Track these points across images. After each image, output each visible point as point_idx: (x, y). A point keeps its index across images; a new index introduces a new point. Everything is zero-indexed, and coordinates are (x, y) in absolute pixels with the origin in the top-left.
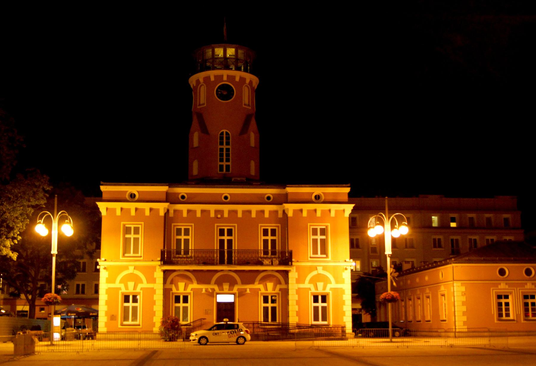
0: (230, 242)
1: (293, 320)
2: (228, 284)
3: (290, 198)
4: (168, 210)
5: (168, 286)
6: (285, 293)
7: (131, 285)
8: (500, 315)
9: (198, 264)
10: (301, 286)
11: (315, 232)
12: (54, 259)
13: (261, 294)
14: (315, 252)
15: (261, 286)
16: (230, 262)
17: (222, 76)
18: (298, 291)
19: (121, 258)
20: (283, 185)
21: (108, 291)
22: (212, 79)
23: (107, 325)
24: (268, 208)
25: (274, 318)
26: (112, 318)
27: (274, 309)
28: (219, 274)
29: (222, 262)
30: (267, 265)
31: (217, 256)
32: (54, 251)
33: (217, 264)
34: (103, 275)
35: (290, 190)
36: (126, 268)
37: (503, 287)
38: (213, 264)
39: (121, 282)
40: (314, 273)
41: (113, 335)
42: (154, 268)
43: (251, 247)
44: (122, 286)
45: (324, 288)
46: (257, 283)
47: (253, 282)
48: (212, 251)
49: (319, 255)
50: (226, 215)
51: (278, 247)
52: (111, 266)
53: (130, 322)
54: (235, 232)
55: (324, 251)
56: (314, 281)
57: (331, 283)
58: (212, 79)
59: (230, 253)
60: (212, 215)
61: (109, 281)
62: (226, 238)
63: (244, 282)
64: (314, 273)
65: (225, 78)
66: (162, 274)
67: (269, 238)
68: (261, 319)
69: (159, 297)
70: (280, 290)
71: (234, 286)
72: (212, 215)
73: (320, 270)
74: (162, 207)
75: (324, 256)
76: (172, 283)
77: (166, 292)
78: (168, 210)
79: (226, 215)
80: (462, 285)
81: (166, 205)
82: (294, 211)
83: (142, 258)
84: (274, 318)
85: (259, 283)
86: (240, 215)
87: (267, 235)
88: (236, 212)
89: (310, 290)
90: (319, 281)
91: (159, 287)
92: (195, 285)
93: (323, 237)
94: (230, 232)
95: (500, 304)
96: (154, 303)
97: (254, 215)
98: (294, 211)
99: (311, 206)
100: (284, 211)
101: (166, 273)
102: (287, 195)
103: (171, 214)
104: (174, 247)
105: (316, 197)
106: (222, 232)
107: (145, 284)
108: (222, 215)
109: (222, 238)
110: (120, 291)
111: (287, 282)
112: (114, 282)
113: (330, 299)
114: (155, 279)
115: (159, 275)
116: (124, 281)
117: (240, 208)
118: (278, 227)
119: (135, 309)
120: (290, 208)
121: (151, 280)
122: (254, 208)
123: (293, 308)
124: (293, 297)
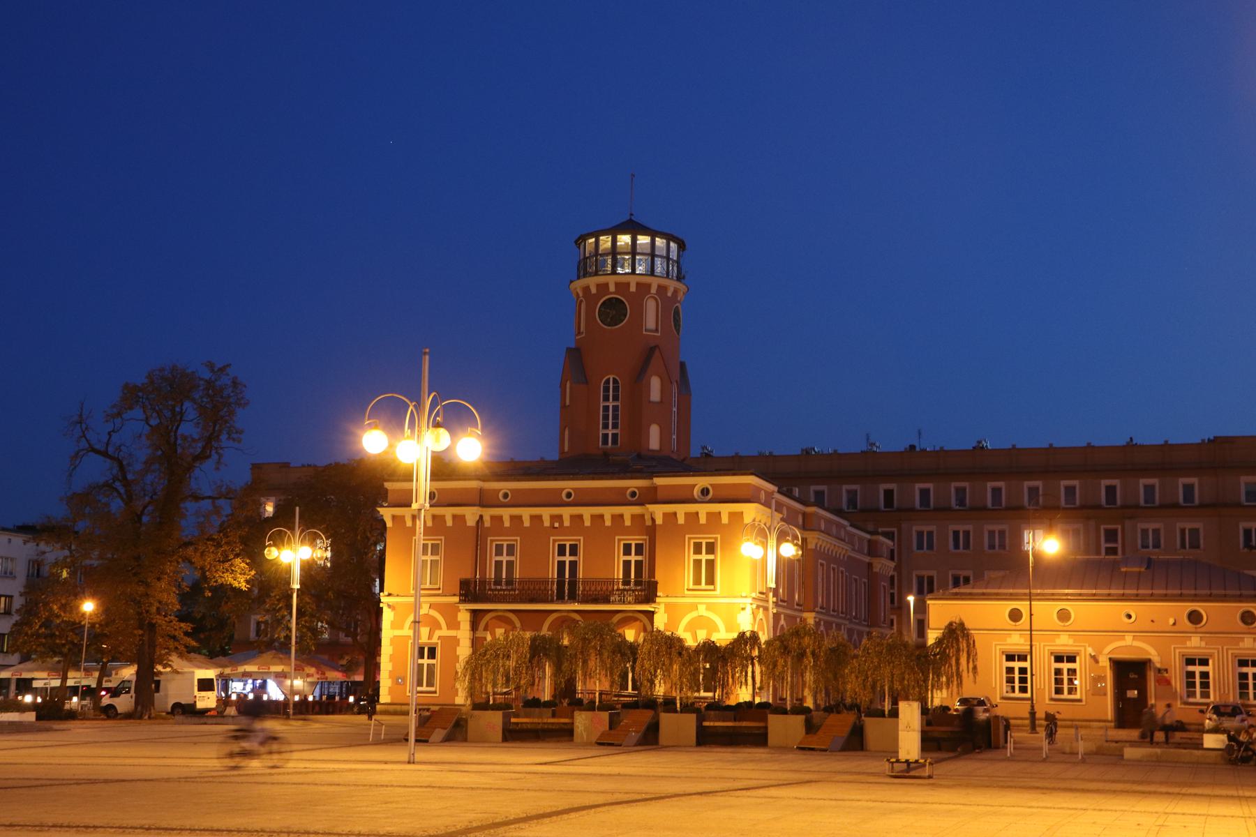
0: (573, 565)
3: (660, 495)
4: (481, 517)
5: (480, 634)
7: (424, 631)
8: (1059, 691)
9: (522, 601)
11: (698, 549)
12: (295, 595)
14: (697, 581)
16: (573, 598)
17: (607, 285)
20: (650, 476)
22: (594, 290)
23: (391, 691)
24: (628, 512)
26: (398, 680)
28: (554, 616)
29: (560, 598)
30: (614, 603)
32: (296, 586)
33: (552, 601)
34: (387, 617)
35: (659, 481)
37: (1195, 644)
40: (694, 614)
41: (274, 692)
43: (602, 575)
48: (546, 581)
49: (703, 586)
50: (567, 523)
52: (401, 604)
53: (424, 688)
55: (711, 580)
57: (718, 631)
58: (594, 290)
59: (573, 583)
60: (547, 523)
61: (394, 625)
62: (568, 559)
64: (694, 614)
65: (612, 288)
67: (633, 558)
72: (547, 523)
73: (702, 610)
74: (470, 515)
75: (711, 587)
76: (486, 629)
78: (481, 517)
79: (567, 523)
81: (475, 509)
82: (665, 515)
86: (587, 523)
87: (630, 554)
88: (580, 517)
90: (701, 628)
91: (464, 634)
93: (711, 557)
98: (665, 515)
99: (691, 508)
101: (476, 616)
102: (655, 489)
103: (487, 523)
105: (702, 491)
106: (562, 550)
107: (445, 632)
108: (561, 522)
109: (572, 558)
112: (401, 627)
114: (459, 623)
115: (464, 617)
117: (587, 512)
118: (619, 540)
120: (658, 511)
121: (453, 624)
122: (608, 512)
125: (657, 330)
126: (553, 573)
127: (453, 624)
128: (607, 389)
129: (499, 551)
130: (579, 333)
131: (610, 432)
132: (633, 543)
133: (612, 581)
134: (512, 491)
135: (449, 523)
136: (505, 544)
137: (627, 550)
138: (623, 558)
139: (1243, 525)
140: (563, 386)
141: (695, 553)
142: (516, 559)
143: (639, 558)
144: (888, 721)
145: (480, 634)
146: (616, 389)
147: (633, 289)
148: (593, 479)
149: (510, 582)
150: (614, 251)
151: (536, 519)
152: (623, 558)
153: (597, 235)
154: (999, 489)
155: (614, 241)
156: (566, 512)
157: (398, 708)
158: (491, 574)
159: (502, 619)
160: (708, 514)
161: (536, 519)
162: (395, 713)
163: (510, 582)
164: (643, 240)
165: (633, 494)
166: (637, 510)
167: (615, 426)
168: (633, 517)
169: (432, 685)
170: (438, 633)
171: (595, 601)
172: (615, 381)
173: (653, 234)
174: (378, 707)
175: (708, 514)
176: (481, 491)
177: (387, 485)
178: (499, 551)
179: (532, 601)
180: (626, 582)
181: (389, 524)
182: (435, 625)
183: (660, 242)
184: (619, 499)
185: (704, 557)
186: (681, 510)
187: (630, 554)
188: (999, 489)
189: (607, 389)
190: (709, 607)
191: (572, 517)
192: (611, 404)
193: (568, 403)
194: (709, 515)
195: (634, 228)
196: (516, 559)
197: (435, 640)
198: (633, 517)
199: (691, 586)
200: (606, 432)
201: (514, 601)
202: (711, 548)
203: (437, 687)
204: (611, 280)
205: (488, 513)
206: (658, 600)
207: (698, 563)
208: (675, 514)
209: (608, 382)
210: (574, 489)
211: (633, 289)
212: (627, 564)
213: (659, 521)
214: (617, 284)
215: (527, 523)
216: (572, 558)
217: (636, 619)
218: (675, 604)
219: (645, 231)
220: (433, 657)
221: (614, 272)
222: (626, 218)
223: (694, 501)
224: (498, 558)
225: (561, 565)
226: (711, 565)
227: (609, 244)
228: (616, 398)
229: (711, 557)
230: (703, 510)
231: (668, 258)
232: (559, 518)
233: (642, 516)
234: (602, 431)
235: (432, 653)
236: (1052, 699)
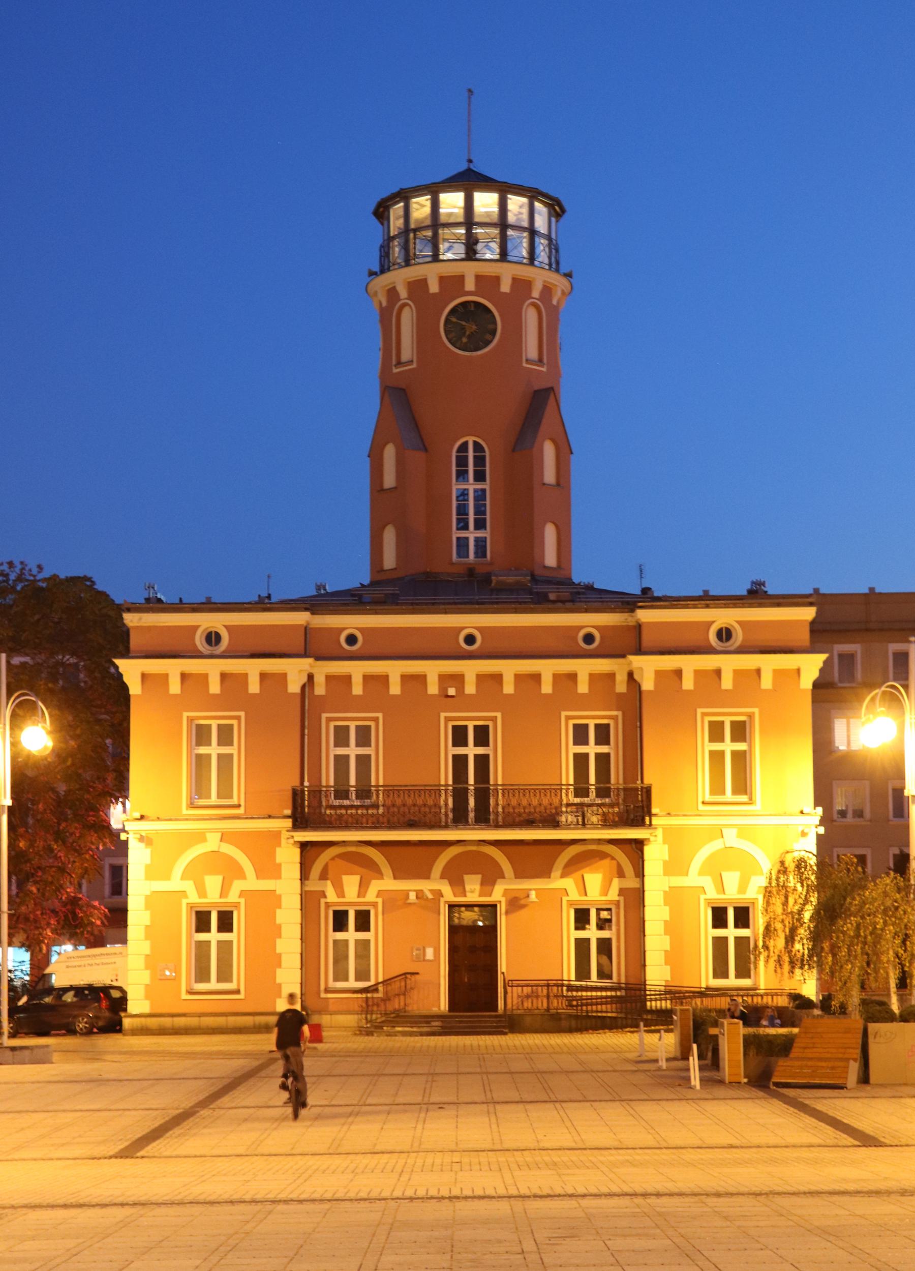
0: (482, 762)
2: (479, 877)
3: (647, 639)
4: (311, 677)
5: (313, 885)
7: (213, 883)
10: (678, 881)
11: (716, 732)
13: (571, 903)
14: (717, 787)
15: (568, 883)
16: (483, 818)
19: (185, 811)
21: (151, 901)
29: (460, 818)
30: (568, 827)
34: (138, 860)
36: (201, 837)
40: (716, 845)
42: (275, 837)
44: (189, 886)
45: (743, 888)
46: (556, 872)
47: (545, 873)
48: (435, 791)
49: (729, 796)
50: (470, 688)
51: (616, 777)
53: (213, 985)
54: (378, 735)
55: (743, 785)
58: (434, 288)
59: (483, 795)
61: (151, 873)
62: (471, 751)
63: (520, 874)
64: (716, 845)
65: (470, 285)
66: (295, 854)
67: (592, 749)
68: (569, 973)
69: (289, 916)
70: (622, 892)
71: (493, 884)
72: (433, 688)
73: (731, 838)
74: (295, 671)
75: (744, 798)
76: (324, 876)
77: (309, 903)
78: (311, 677)
79: (470, 688)
82: (659, 674)
83: (241, 811)
85: (563, 876)
86: (395, 689)
87: (465, 744)
88: (421, 679)
89: (186, 897)
90: (729, 869)
91: (288, 886)
92: (389, 883)
94: (364, 737)
100: (631, 675)
103: (320, 689)
105: (719, 634)
106: (459, 736)
107: (252, 882)
109: (481, 750)
110: (184, 902)
111: (640, 873)
112: (167, 877)
115: (288, 857)
118: (238, 718)
120: (648, 668)
121: (268, 868)
124: (656, 913)
125: (540, 360)
126: (446, 776)
127: (268, 868)
128: (462, 461)
129: (341, 737)
130: (527, 360)
131: (472, 535)
132: (592, 724)
133: (557, 789)
135: (254, 687)
136: (353, 725)
137: (580, 735)
141: (712, 739)
142: (376, 751)
143: (604, 749)
145: (313, 885)
146: (480, 461)
147: (505, 287)
148: (516, 611)
150: (436, 221)
153: (434, 190)
155: (435, 205)
156: (471, 669)
157: (167, 1022)
158: (328, 778)
159: (356, 859)
160: (736, 672)
161: (415, 681)
162: (162, 1032)
163: (364, 792)
164: (486, 202)
165: (470, 640)
166: (602, 665)
167: (480, 524)
168: (594, 678)
169: (229, 979)
170: (238, 886)
171: (529, 823)
172: (478, 447)
173: (504, 189)
174: (127, 1022)
175: (736, 672)
176: (306, 629)
177: (130, 619)
178: (341, 737)
179: (412, 825)
180: (581, 791)
181: (135, 688)
183: (517, 204)
184: (470, 648)
185: (728, 747)
186: (689, 664)
187: (465, 744)
189: (462, 461)
190: (744, 832)
191: (557, 678)
192: (472, 486)
193: (389, 480)
194: (739, 674)
195: (470, 180)
196: (376, 751)
197: (233, 897)
198: (594, 678)
199: (708, 798)
200: (463, 534)
201: (376, 827)
202: (740, 731)
203: (239, 979)
204: (470, 270)
205: (324, 670)
206: (655, 821)
207: (717, 758)
208: (758, 672)
209: (464, 447)
210: (360, 630)
211: (505, 287)
212: (581, 761)
213: (648, 684)
214: (479, 278)
215: (395, 689)
216: (481, 750)
217: (603, 856)
218: (681, 829)
219: (486, 183)
220: (746, 925)
221: (435, 258)
222: (463, 166)
223: (708, 650)
224: (341, 751)
225: (460, 762)
226: (741, 761)
227: (427, 210)
228: (480, 476)
229: (741, 746)
230: (729, 664)
231: (533, 232)
232: (458, 679)
233: (611, 676)
234: (456, 534)
235: (226, 923)
236: (191, 992)
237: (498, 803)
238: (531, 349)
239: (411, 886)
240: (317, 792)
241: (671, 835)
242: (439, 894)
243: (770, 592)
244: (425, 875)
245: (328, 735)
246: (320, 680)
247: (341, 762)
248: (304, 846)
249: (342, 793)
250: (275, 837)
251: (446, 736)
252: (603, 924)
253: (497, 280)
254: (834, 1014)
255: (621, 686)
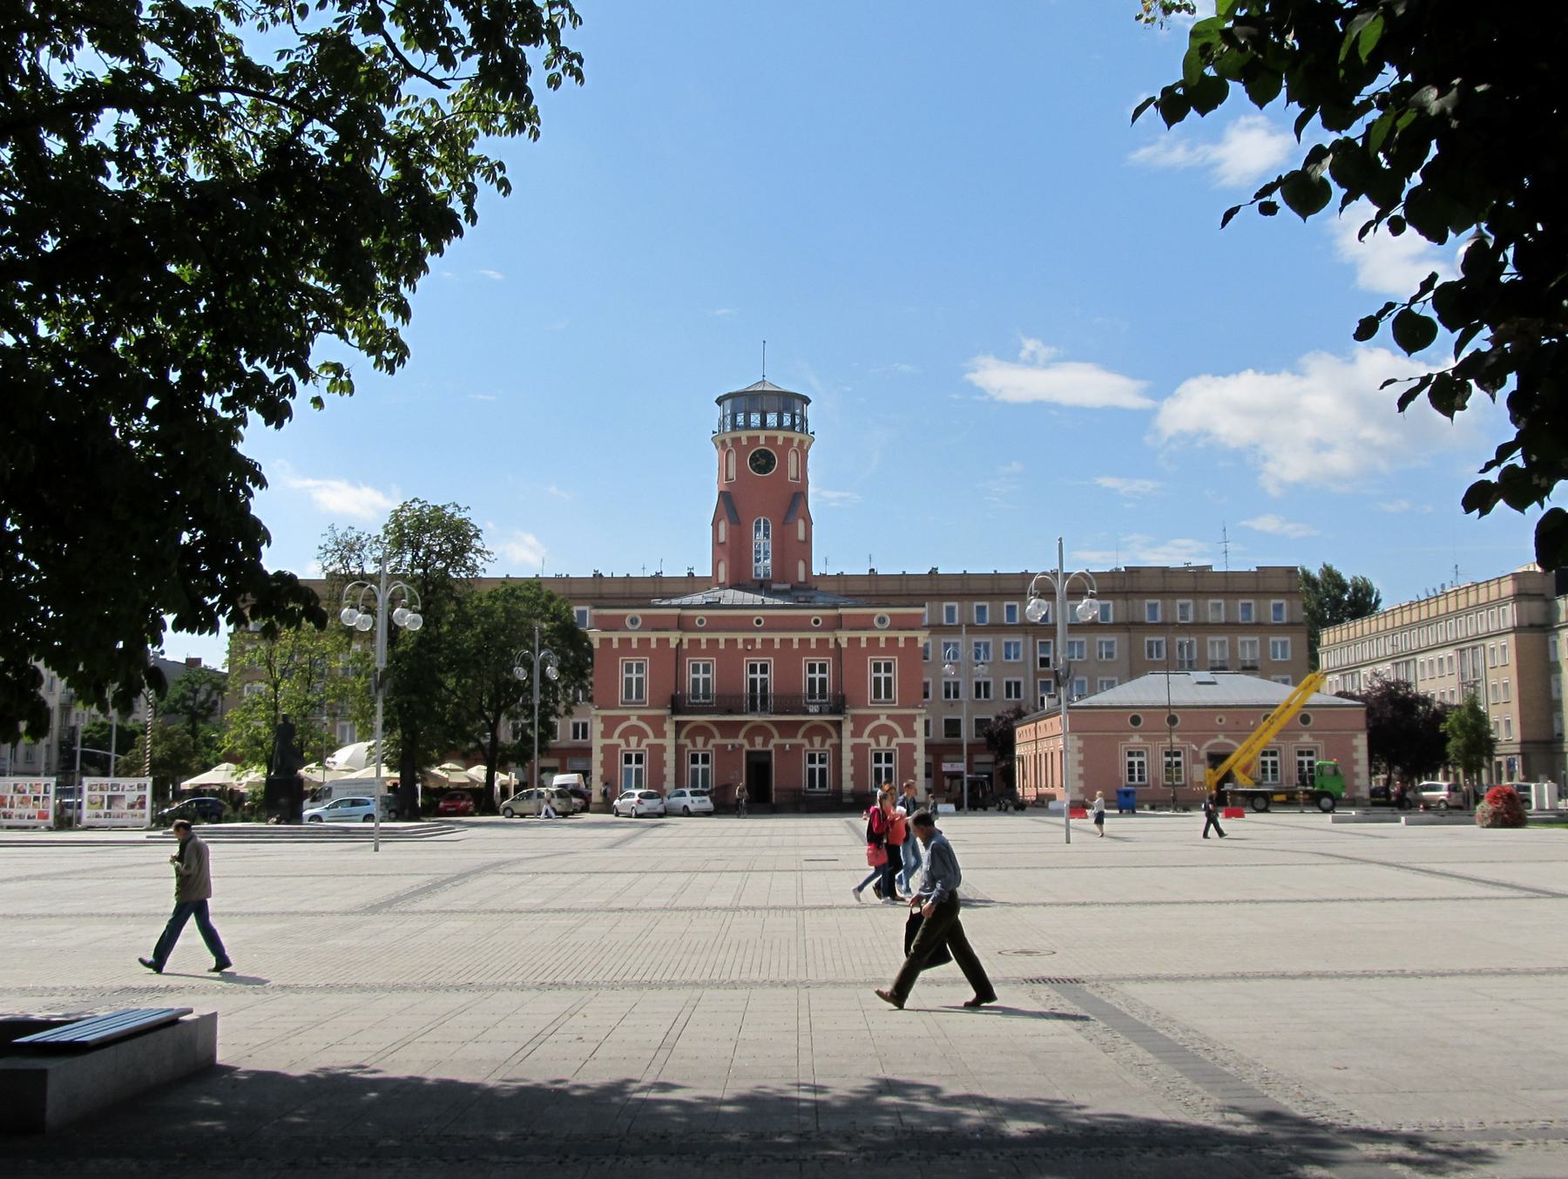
1: (848, 785)
5: (683, 741)
6: (838, 749)
14: (877, 695)
16: (764, 709)
18: (855, 748)
25: (822, 784)
27: (822, 771)
29: (753, 709)
31: (747, 703)
38: (740, 713)
39: (870, 736)
40: (876, 723)
42: (662, 719)
51: (829, 688)
54: (896, 667)
56: (625, 735)
58: (744, 442)
59: (764, 699)
64: (876, 723)
65: (762, 441)
66: (673, 727)
68: (805, 783)
69: (670, 757)
72: (615, 645)
74: (674, 637)
77: (679, 750)
79: (758, 646)
80: (1080, 738)
84: (822, 784)
86: (901, 645)
91: (669, 742)
95: (1131, 764)
96: (663, 764)
97: (615, 645)
101: (679, 726)
103: (685, 646)
104: (689, 688)
107: (652, 740)
111: (840, 736)
113: (896, 757)
115: (669, 728)
116: (875, 734)
119: (889, 771)
120: (844, 637)
121: (660, 734)
123: (847, 770)
124: (847, 756)
126: (746, 689)
127: (660, 734)
134: (708, 617)
138: (626, 676)
139: (1147, 639)
140: (715, 524)
144: (1529, 738)
147: (780, 442)
149: (706, 696)
151: (854, 642)
152: (626, 676)
154: (984, 608)
158: (689, 688)
161: (854, 642)
165: (759, 622)
166: (823, 635)
170: (645, 742)
178: (877, 668)
182: (642, 734)
188: (984, 608)
197: (893, 746)
204: (762, 435)
205: (687, 637)
211: (780, 442)
213: (844, 645)
223: (872, 628)
237: (771, 702)
238: (792, 472)
239: (729, 742)
240: (683, 696)
241: (855, 718)
242: (742, 746)
243: (224, 766)
244: (795, 737)
245: (689, 667)
246: (685, 641)
247: (696, 681)
248: (677, 723)
249: (696, 696)
250: (662, 719)
251: (870, 667)
252: (822, 761)
253: (776, 438)
254: (1041, 804)
255: (832, 646)
